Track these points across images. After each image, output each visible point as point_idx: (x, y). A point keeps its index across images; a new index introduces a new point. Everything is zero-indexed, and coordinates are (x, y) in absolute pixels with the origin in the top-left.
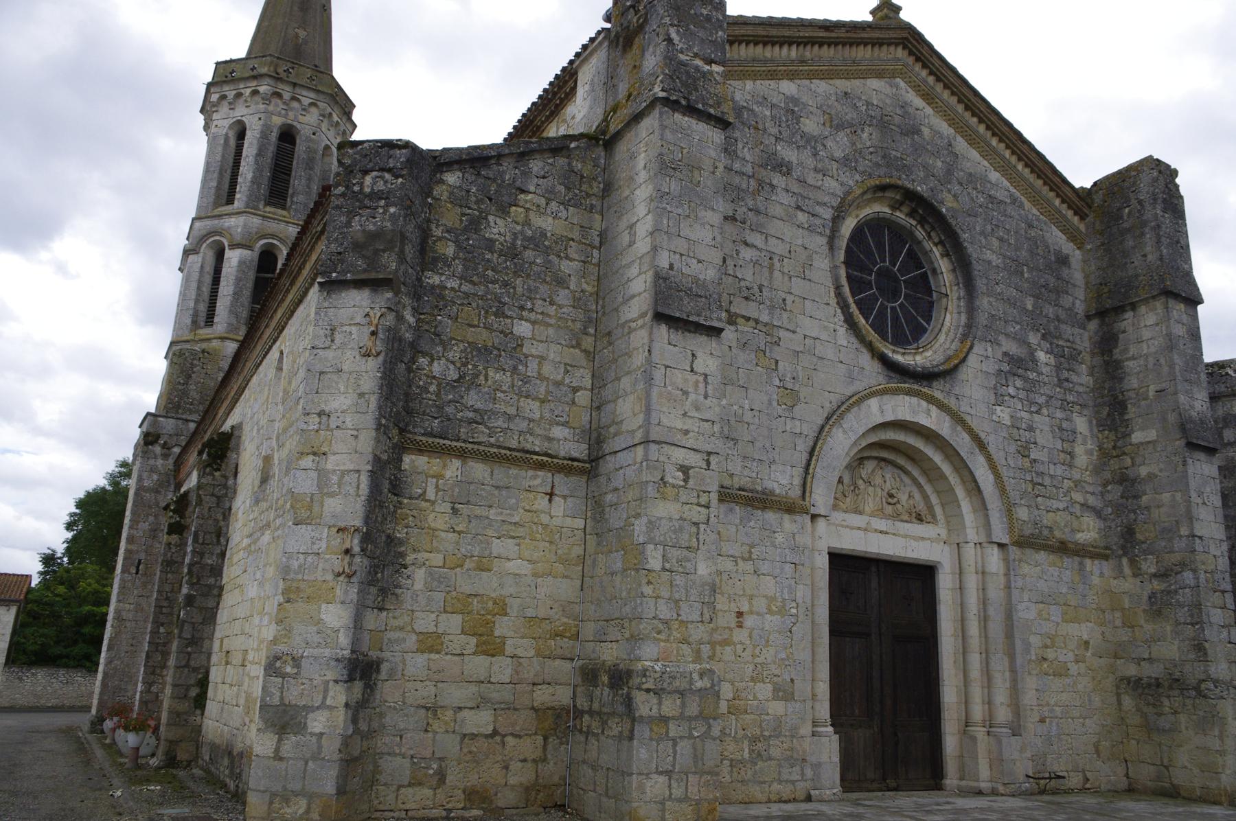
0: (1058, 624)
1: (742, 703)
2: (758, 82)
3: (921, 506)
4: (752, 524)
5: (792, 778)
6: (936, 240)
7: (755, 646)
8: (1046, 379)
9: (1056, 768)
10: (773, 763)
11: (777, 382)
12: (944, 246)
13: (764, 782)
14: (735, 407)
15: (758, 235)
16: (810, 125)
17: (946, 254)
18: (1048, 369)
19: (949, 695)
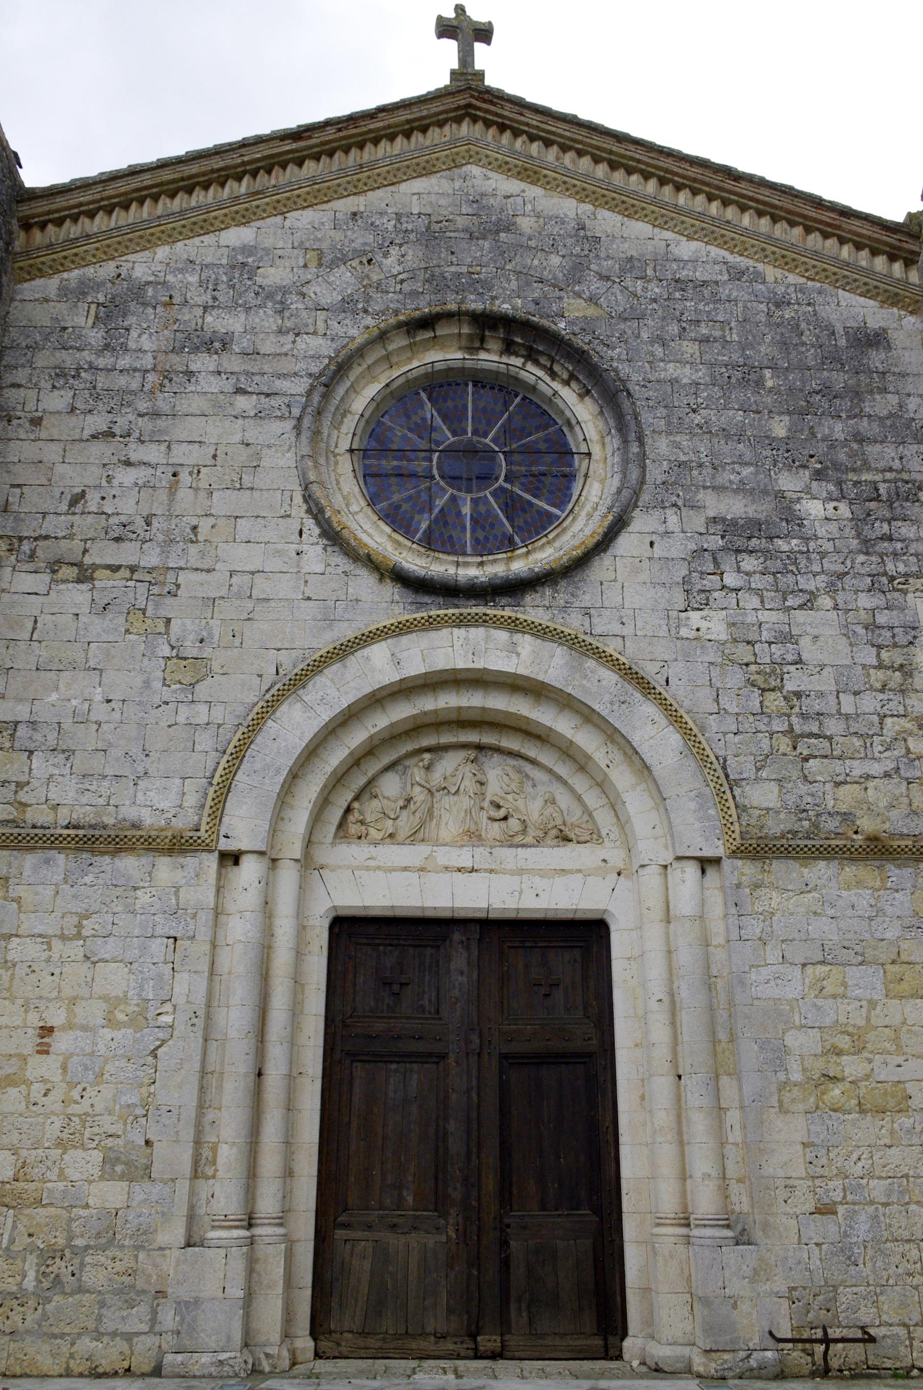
0: (872, 1004)
1: (32, 1186)
2: (180, 244)
3: (576, 816)
4: (88, 879)
5: (127, 1329)
6: (565, 376)
7: (72, 1085)
8: (829, 546)
9: (866, 1315)
10: (86, 1298)
11: (166, 651)
12: (578, 380)
13: (62, 1336)
14: (74, 702)
15: (154, 446)
16: (273, 275)
17: (585, 393)
18: (833, 527)
19: (632, 1164)
